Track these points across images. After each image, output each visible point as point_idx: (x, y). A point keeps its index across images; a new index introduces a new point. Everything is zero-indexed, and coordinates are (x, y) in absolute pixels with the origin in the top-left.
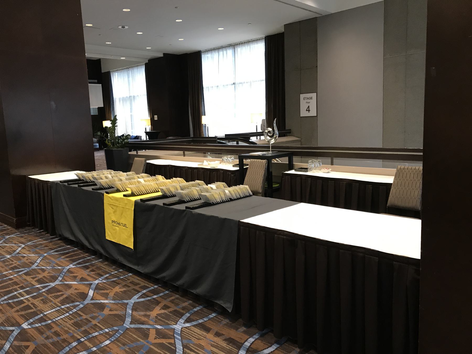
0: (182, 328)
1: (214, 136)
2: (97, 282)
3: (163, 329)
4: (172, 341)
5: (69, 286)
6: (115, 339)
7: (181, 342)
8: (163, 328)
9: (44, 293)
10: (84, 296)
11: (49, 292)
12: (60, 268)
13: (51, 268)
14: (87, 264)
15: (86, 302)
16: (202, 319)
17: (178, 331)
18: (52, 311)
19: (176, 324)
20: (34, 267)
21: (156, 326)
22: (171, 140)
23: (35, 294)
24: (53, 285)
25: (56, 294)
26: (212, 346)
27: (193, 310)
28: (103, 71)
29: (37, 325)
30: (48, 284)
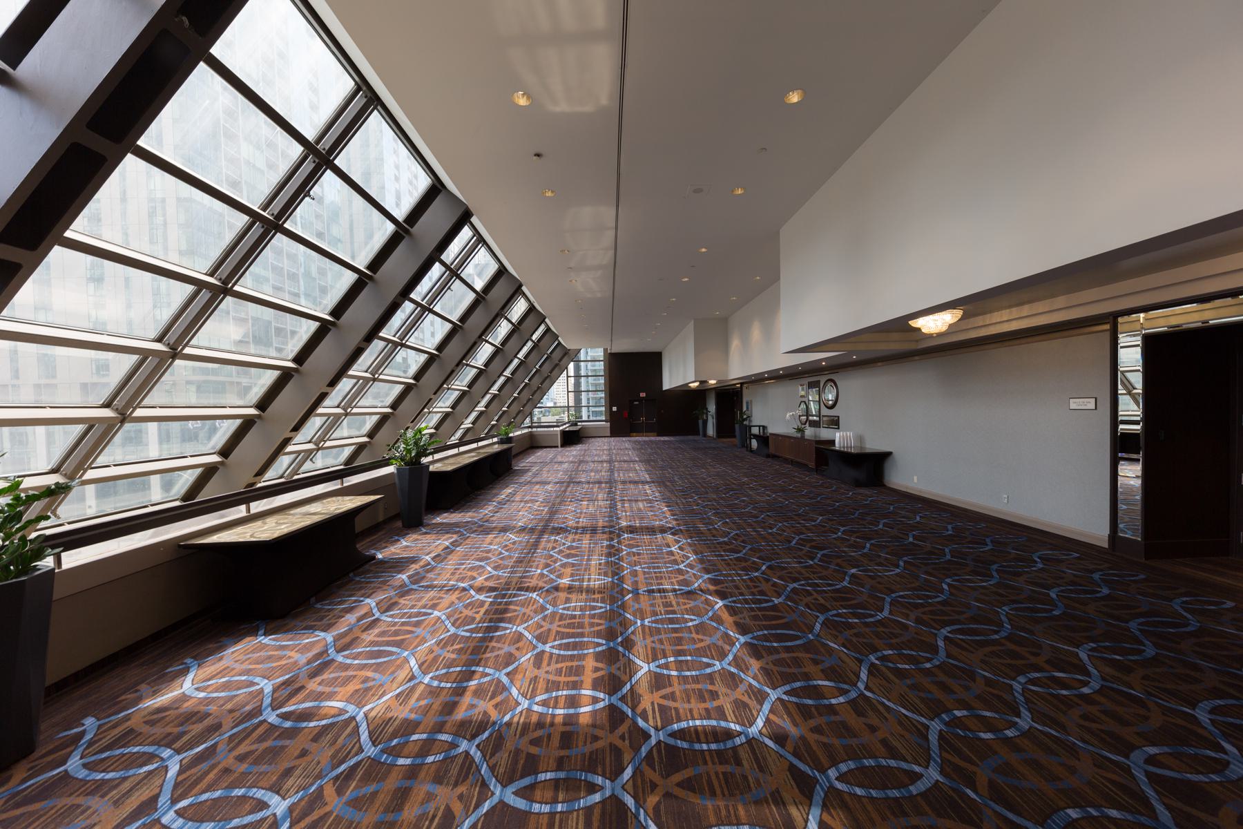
2: (756, 574)
5: (780, 578)
10: (769, 567)
14: (759, 597)
15: (769, 563)
16: (889, 766)
20: (453, 630)
22: (116, 529)
26: (886, 718)
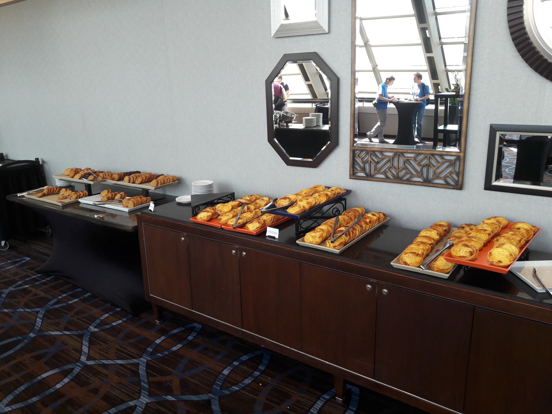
0: (140, 398)
1: (356, 77)
3: (164, 396)
4: (151, 379)
6: (219, 377)
7: (141, 378)
8: (163, 396)
9: (19, 280)
10: (48, 315)
11: (14, 282)
12: (6, 310)
13: (18, 310)
17: (144, 393)
18: (8, 268)
19: (147, 403)
21: (174, 399)
23: (28, 279)
24: (11, 289)
25: (6, 280)
27: (55, 387)
28: (35, 160)
29: (18, 259)
30: (17, 289)
